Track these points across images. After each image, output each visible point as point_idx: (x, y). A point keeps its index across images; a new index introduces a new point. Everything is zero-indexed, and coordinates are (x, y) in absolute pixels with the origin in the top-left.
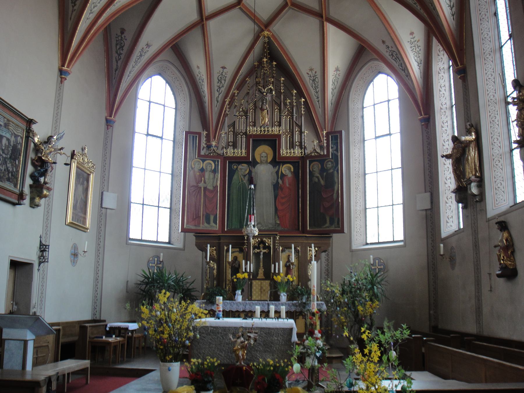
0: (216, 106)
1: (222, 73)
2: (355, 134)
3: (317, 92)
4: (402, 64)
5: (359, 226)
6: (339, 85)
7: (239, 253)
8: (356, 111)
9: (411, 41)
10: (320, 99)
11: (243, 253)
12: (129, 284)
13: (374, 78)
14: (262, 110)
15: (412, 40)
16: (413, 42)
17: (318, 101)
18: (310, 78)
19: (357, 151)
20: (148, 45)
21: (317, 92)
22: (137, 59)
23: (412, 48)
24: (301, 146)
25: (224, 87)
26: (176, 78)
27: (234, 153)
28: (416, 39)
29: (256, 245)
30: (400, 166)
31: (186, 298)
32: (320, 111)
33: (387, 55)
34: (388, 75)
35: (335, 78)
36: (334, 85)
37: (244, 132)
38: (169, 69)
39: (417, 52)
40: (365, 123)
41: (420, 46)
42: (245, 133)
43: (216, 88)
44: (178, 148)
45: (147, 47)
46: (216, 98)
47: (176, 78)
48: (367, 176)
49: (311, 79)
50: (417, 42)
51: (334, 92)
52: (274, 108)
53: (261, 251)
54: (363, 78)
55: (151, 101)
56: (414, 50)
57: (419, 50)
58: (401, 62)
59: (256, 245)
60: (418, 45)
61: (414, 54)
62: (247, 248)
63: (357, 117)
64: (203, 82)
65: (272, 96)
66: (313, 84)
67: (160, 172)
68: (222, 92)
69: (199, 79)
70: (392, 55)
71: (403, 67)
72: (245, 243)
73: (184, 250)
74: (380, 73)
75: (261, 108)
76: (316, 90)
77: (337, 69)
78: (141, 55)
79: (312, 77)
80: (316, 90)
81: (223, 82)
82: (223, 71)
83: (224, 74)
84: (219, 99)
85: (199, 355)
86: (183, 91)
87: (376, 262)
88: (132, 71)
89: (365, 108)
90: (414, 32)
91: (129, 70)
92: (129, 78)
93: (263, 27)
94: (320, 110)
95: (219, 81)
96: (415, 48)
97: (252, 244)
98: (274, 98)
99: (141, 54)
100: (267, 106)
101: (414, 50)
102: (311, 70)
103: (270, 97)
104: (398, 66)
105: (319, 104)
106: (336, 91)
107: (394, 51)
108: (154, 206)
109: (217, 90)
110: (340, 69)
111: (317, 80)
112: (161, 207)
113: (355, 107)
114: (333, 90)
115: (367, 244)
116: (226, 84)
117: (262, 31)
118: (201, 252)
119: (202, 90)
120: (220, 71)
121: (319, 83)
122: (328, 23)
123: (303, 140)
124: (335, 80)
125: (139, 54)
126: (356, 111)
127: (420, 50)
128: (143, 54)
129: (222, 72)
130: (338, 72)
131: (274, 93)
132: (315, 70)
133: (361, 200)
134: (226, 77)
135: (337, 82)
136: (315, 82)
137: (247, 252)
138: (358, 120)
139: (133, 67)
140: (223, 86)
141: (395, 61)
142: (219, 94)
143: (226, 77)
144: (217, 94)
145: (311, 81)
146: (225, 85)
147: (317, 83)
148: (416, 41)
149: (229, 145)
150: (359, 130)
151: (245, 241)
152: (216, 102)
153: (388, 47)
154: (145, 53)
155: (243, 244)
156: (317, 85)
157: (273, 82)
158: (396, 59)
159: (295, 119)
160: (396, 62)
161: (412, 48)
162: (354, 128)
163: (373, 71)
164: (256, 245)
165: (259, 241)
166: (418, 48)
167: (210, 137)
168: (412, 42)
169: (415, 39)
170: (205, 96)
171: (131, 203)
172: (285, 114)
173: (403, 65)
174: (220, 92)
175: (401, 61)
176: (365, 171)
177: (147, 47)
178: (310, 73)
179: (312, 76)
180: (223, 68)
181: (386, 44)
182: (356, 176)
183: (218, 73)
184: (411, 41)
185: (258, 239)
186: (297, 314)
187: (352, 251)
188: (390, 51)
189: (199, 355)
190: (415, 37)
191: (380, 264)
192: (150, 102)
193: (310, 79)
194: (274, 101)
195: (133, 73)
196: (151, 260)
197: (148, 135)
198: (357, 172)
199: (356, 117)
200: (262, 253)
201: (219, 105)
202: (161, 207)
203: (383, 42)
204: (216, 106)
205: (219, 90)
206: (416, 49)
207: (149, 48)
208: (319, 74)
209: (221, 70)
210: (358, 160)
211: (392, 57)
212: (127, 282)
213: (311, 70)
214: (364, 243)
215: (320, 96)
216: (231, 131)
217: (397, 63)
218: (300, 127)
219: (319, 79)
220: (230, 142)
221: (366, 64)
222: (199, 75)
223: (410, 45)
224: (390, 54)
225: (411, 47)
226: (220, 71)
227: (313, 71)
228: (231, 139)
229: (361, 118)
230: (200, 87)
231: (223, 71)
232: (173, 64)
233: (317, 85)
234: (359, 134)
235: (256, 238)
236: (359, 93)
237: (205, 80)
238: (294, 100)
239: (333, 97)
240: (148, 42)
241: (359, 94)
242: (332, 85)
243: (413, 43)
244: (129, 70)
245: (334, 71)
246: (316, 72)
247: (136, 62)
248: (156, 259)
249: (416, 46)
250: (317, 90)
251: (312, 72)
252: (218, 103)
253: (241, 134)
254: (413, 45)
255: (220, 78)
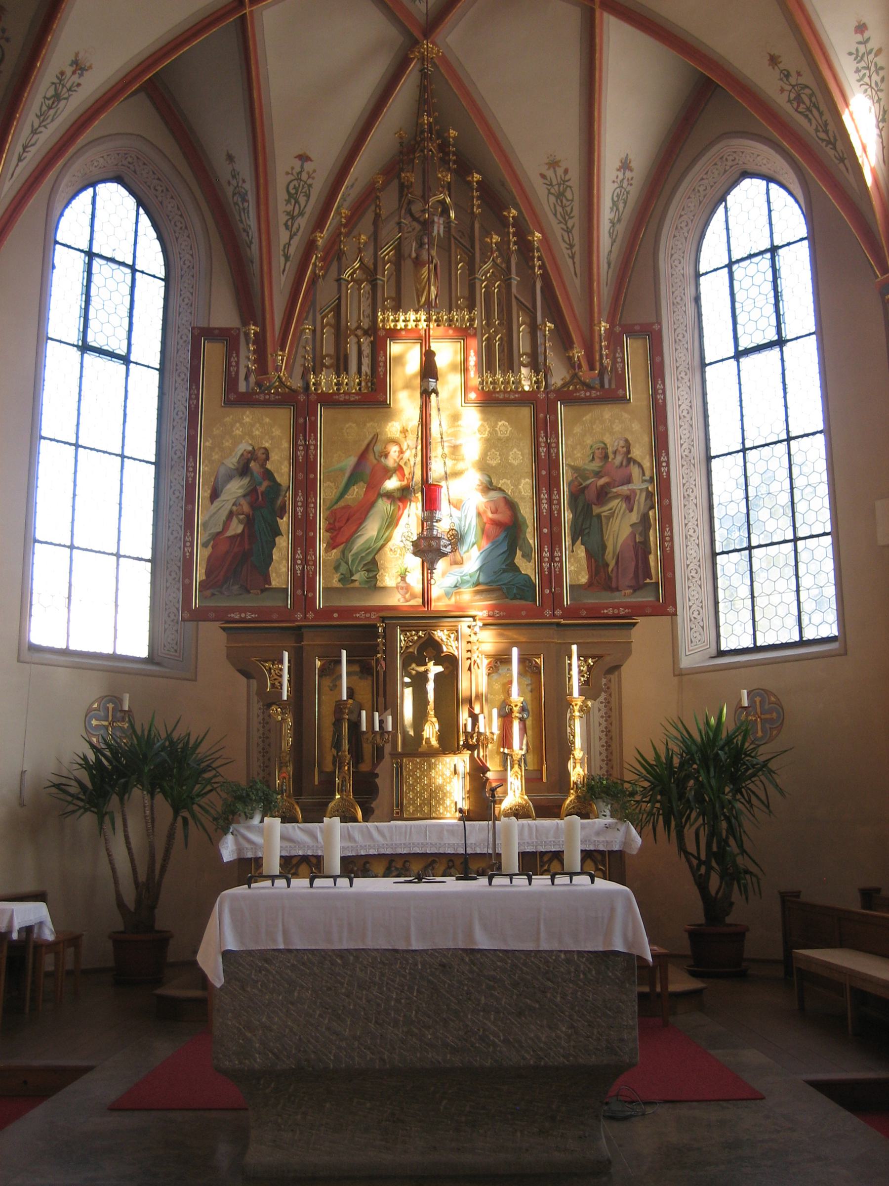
0: (284, 270)
1: (298, 174)
2: (678, 347)
3: (569, 231)
4: (826, 124)
5: (698, 603)
6: (628, 211)
7: (360, 678)
8: (680, 284)
9: (857, 50)
10: (576, 248)
11: (370, 678)
12: (27, 777)
13: (728, 192)
14: (418, 263)
15: (862, 49)
16: (864, 54)
17: (573, 257)
18: (549, 190)
19: (684, 393)
20: (79, 67)
21: (569, 231)
22: (44, 108)
23: (861, 74)
24: (535, 366)
25: (306, 216)
26: (167, 190)
27: (338, 384)
28: (873, 44)
29: (414, 650)
30: (821, 427)
31: (713, 782)
32: (575, 285)
33: (781, 100)
34: (769, 179)
35: (618, 190)
36: (617, 209)
37: (366, 327)
38: (144, 164)
39: (873, 85)
40: (704, 318)
41: (882, 68)
42: (369, 329)
43: (283, 218)
44: (176, 389)
45: (74, 73)
46: (282, 247)
47: (167, 190)
48: (714, 462)
49: (552, 191)
50: (876, 55)
51: (615, 233)
52: (453, 259)
53: (426, 672)
54: (699, 191)
55: (95, 250)
56: (867, 80)
57: (878, 79)
58: (824, 118)
59: (414, 650)
60: (876, 65)
61: (866, 91)
62: (384, 659)
63: (682, 299)
64: (244, 200)
65: (448, 223)
66: (557, 206)
67: (123, 456)
68: (298, 230)
69: (234, 194)
70: (798, 99)
71: (831, 134)
72: (378, 645)
73: (195, 680)
74: (746, 174)
75: (417, 258)
76: (566, 225)
77: (625, 165)
78: (57, 97)
79: (556, 187)
80: (566, 225)
81: (302, 200)
82: (302, 167)
83: (304, 176)
84: (292, 251)
85: (249, 1035)
86: (186, 228)
87: (755, 702)
88: (33, 145)
89: (703, 274)
90: (869, 25)
91: (22, 141)
92: (22, 165)
93: (417, 34)
94: (577, 282)
95: (292, 197)
96: (867, 72)
97: (401, 648)
98: (453, 232)
99: (56, 90)
100: (434, 253)
101: (867, 80)
102: (553, 164)
103: (442, 227)
104: (813, 133)
105: (574, 263)
106: (620, 228)
107: (807, 87)
108: (104, 553)
109: (286, 225)
110: (632, 165)
111: (568, 194)
112: (125, 556)
113: (674, 273)
114: (612, 222)
115: (721, 654)
116: (311, 206)
117: (415, 43)
118: (245, 679)
119: (241, 226)
120: (293, 168)
121: (576, 205)
122: (606, 15)
123: (541, 350)
124: (618, 196)
125: (51, 92)
126: (680, 284)
127: (883, 80)
128: (64, 93)
129: (299, 170)
130: (628, 174)
131: (452, 215)
132: (564, 165)
133: (699, 530)
134: (310, 186)
135: (625, 203)
136: (564, 201)
137: (385, 672)
138: (684, 308)
139: (34, 132)
140: (301, 214)
141: (806, 116)
142: (291, 238)
143: (310, 186)
144: (284, 236)
145: (552, 199)
146: (308, 210)
147: (568, 203)
148: (872, 50)
149: (323, 365)
150: (688, 336)
151: (379, 640)
152: (282, 260)
153: (788, 76)
154: (70, 90)
155: (374, 650)
156: (568, 209)
157: (449, 183)
158: (811, 112)
159: (514, 290)
160: (810, 121)
161: (861, 74)
162: (675, 330)
163: (725, 171)
164: (411, 650)
165: (420, 637)
166: (878, 74)
167: (265, 342)
168: (860, 54)
169: (869, 46)
170: (251, 242)
171: (36, 541)
172: (485, 274)
173: (831, 127)
174: (294, 229)
175: (827, 116)
176: (708, 448)
177: (74, 73)
178: (550, 174)
179: (555, 182)
180: (304, 158)
181: (782, 66)
182: (684, 463)
183: (287, 173)
184: (857, 50)
185: (417, 632)
186: (546, 859)
187: (680, 674)
188: (793, 86)
189: (249, 1035)
190: (868, 40)
191: (766, 707)
192: (90, 255)
193: (550, 193)
194: (452, 239)
195: (33, 150)
196: (95, 709)
197: (85, 347)
198: (687, 452)
199: (678, 299)
200: (431, 676)
201: (292, 267)
202: (125, 556)
203: (774, 60)
204: (284, 270)
205: (290, 223)
206: (870, 77)
207: (81, 75)
208: (575, 177)
209: (297, 163)
210: (688, 419)
211: (798, 106)
212: (23, 773)
213: (553, 164)
214: (713, 651)
215: (576, 241)
216: (328, 324)
217: (814, 121)
218: (531, 314)
219: (574, 194)
220: (327, 355)
221: (712, 144)
222: (234, 182)
223: (854, 65)
224: (792, 96)
225: (858, 71)
226: (293, 168)
227: (557, 169)
228: (328, 348)
229: (693, 304)
230: (238, 218)
231: (302, 167)
232: (160, 151)
233: (568, 209)
234: (690, 346)
235: (411, 631)
236: (686, 234)
237: (249, 193)
238: (511, 244)
239: (612, 245)
240: (77, 54)
241: (686, 239)
242: (612, 209)
243: (862, 59)
244: (22, 141)
245: (618, 170)
246: (566, 171)
247: (42, 116)
248: (111, 706)
249: (873, 69)
250: (570, 223)
251: (555, 172)
252: (288, 264)
253: (359, 332)
254: (863, 64)
255: (295, 188)
